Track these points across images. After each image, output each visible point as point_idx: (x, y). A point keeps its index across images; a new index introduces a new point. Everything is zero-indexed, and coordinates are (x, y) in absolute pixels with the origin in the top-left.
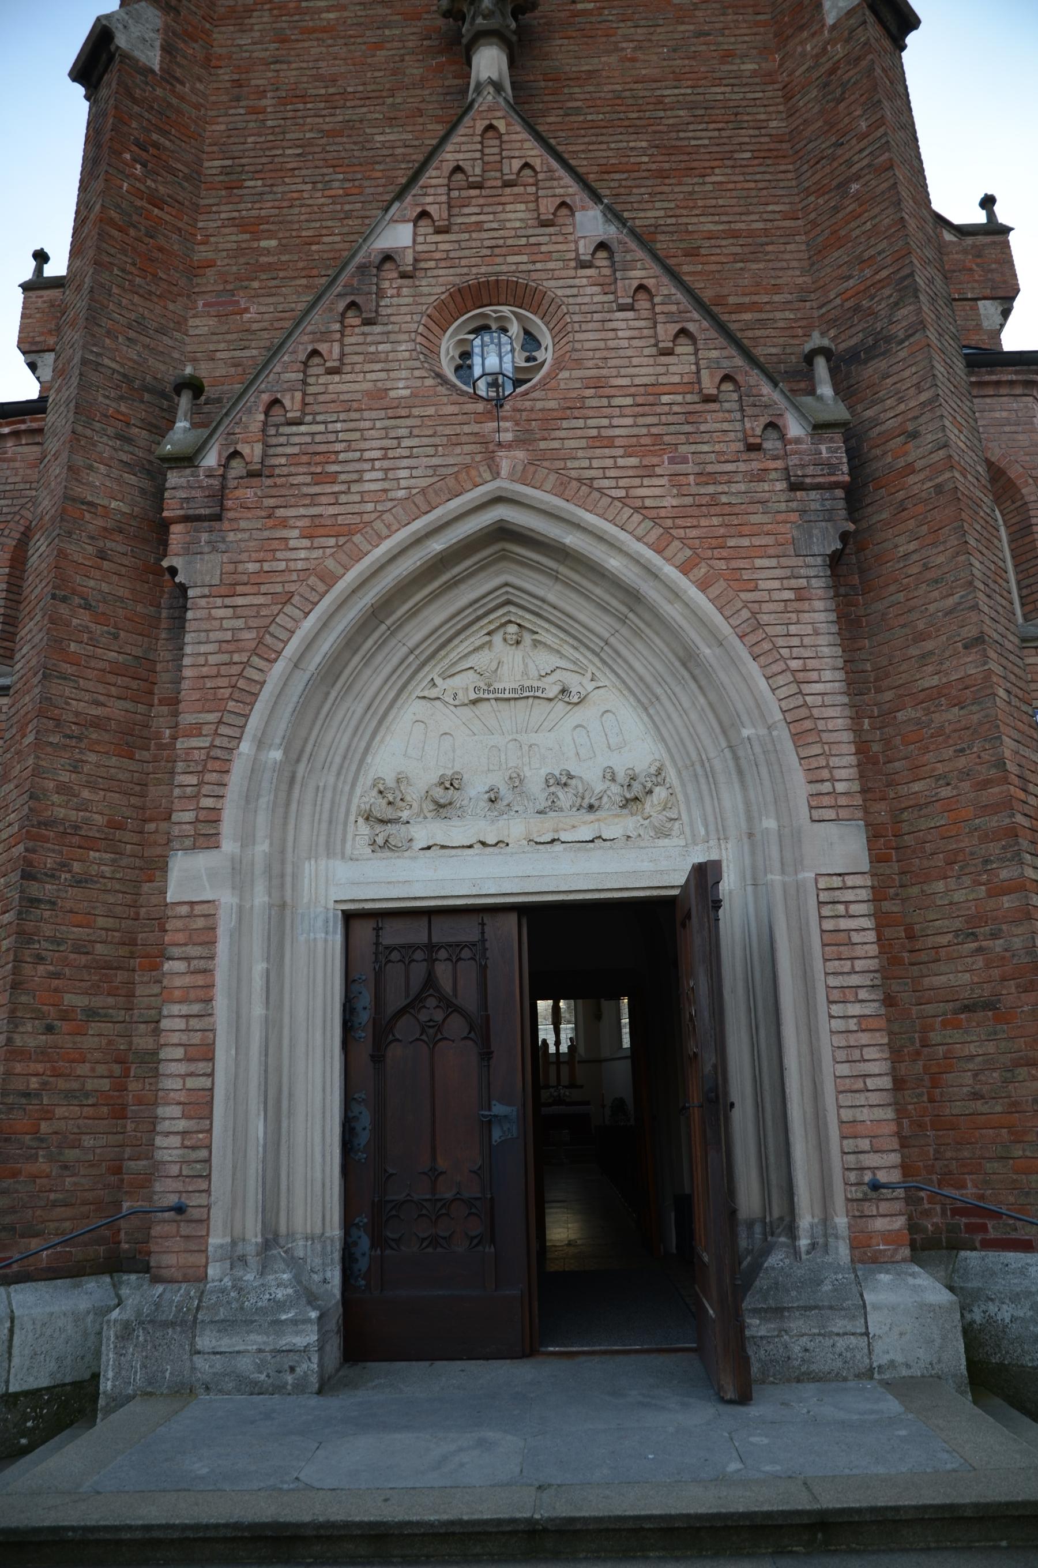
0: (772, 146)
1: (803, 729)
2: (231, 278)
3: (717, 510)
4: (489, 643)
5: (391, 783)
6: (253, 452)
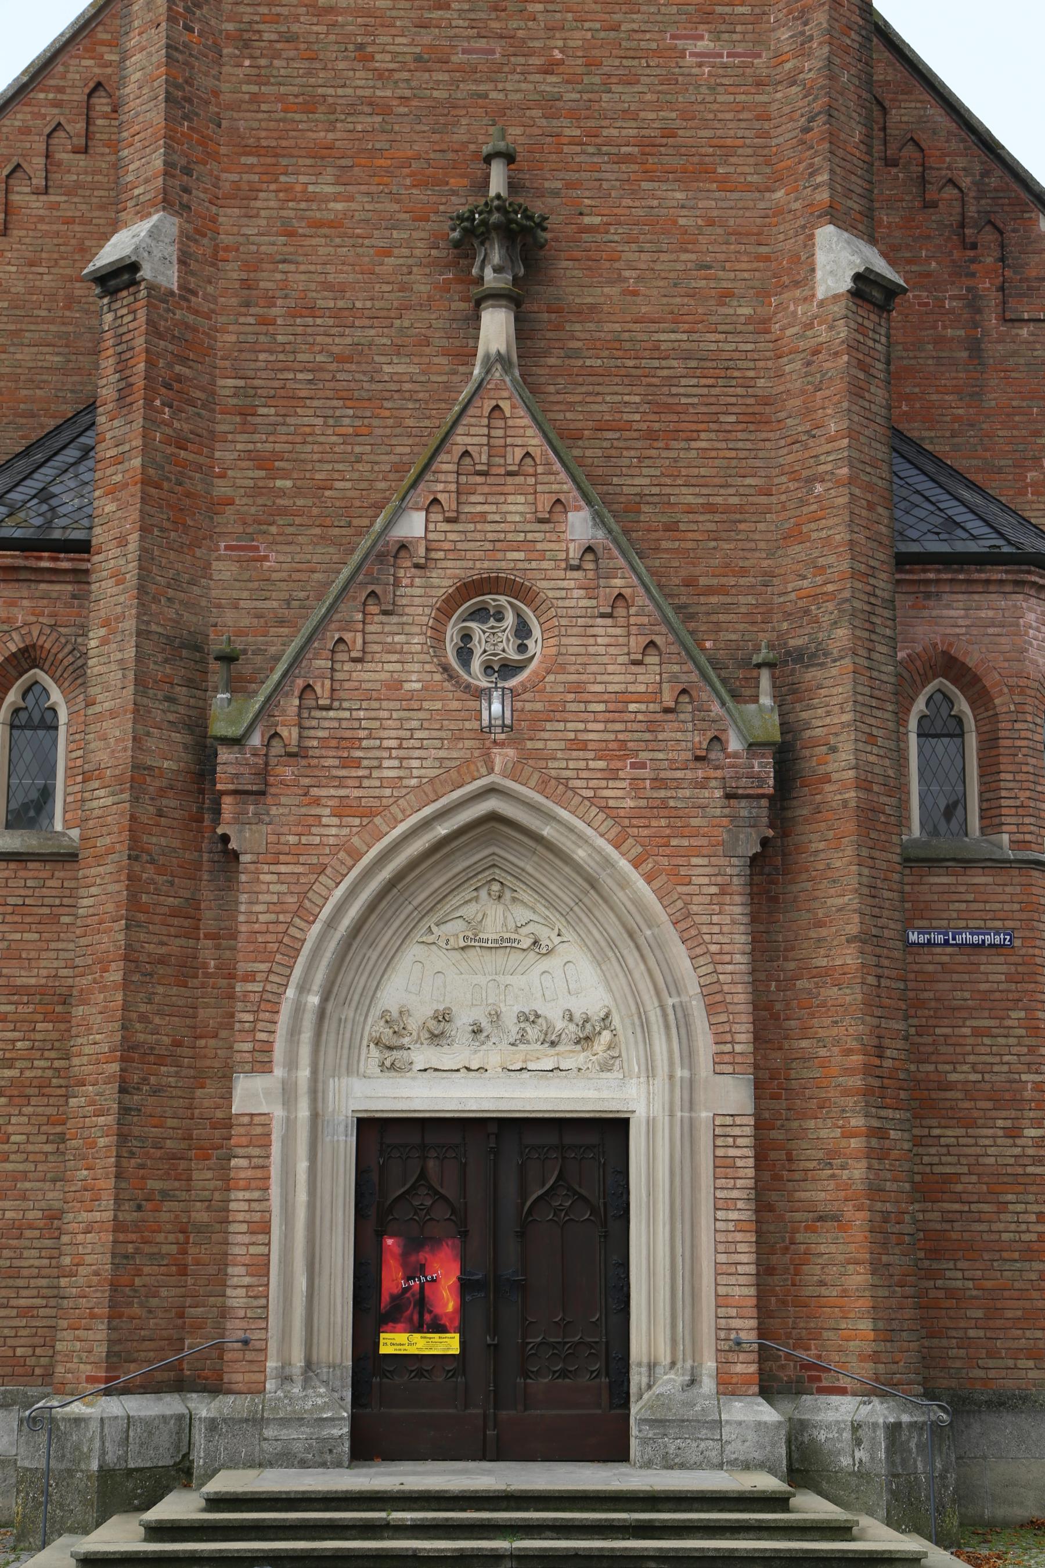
0: (757, 409)
1: (715, 1002)
2: (249, 520)
3: (666, 813)
4: (476, 899)
5: (395, 1014)
6: (290, 734)
